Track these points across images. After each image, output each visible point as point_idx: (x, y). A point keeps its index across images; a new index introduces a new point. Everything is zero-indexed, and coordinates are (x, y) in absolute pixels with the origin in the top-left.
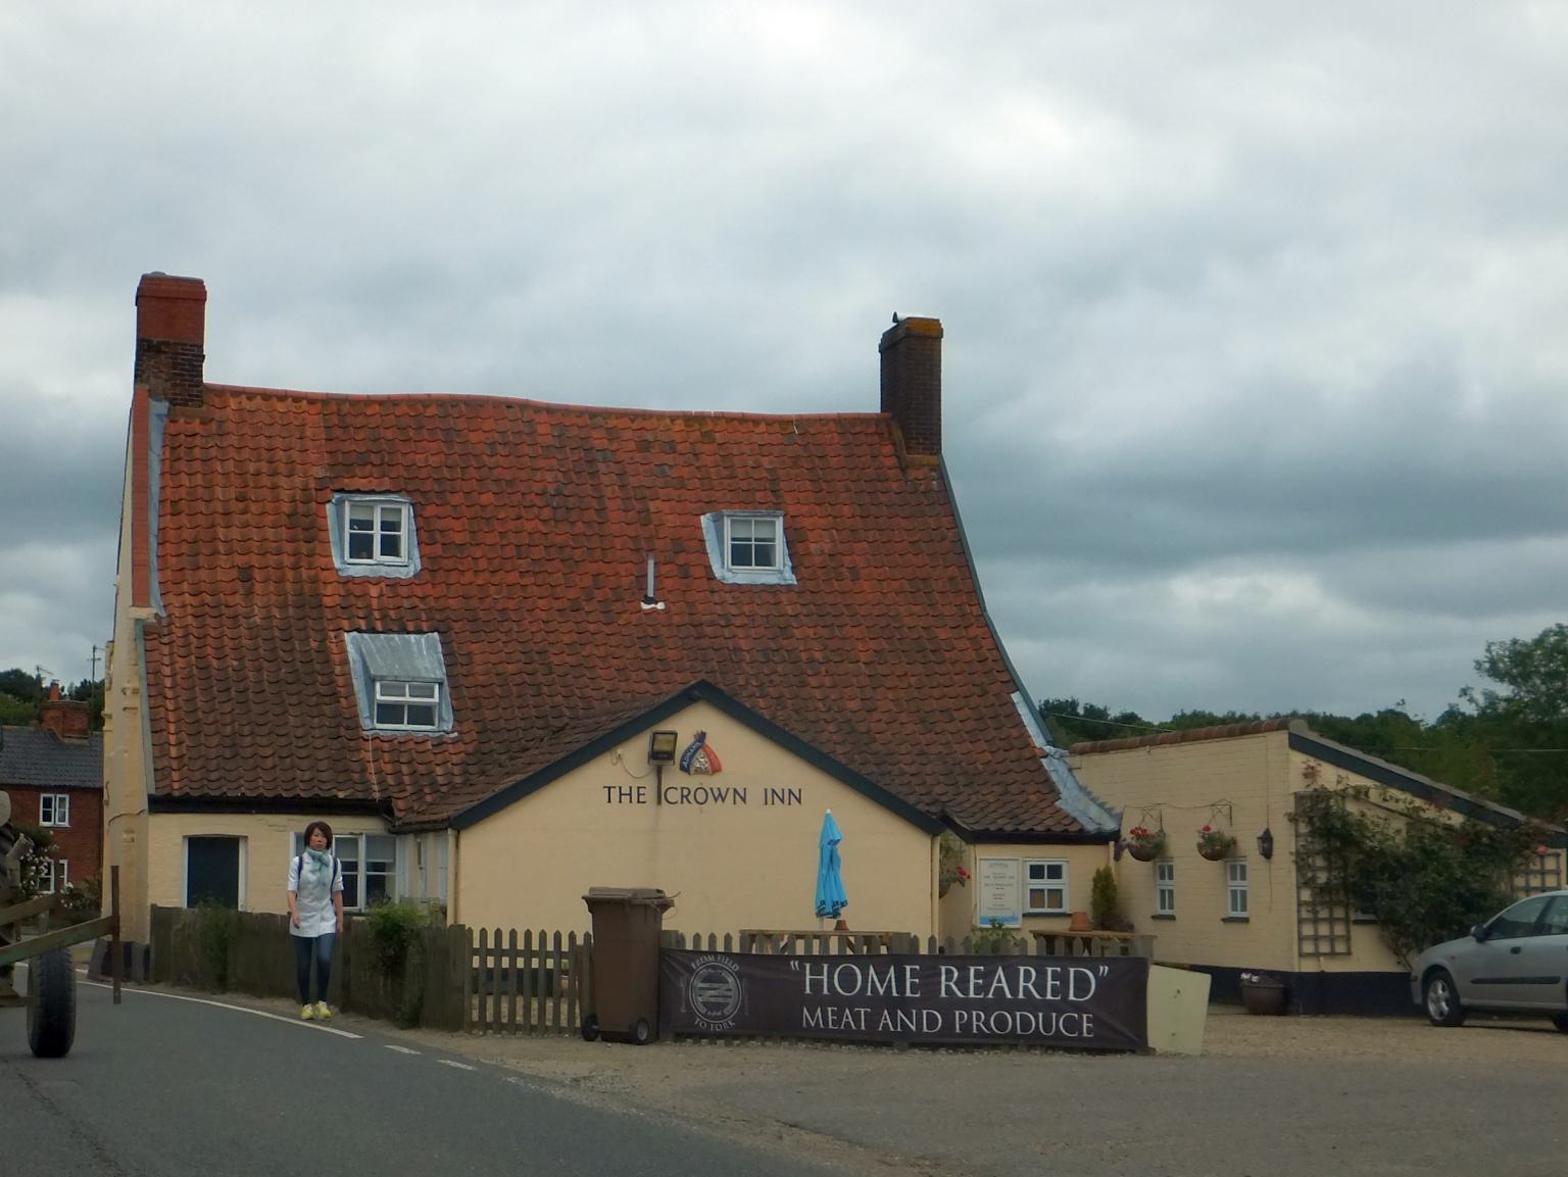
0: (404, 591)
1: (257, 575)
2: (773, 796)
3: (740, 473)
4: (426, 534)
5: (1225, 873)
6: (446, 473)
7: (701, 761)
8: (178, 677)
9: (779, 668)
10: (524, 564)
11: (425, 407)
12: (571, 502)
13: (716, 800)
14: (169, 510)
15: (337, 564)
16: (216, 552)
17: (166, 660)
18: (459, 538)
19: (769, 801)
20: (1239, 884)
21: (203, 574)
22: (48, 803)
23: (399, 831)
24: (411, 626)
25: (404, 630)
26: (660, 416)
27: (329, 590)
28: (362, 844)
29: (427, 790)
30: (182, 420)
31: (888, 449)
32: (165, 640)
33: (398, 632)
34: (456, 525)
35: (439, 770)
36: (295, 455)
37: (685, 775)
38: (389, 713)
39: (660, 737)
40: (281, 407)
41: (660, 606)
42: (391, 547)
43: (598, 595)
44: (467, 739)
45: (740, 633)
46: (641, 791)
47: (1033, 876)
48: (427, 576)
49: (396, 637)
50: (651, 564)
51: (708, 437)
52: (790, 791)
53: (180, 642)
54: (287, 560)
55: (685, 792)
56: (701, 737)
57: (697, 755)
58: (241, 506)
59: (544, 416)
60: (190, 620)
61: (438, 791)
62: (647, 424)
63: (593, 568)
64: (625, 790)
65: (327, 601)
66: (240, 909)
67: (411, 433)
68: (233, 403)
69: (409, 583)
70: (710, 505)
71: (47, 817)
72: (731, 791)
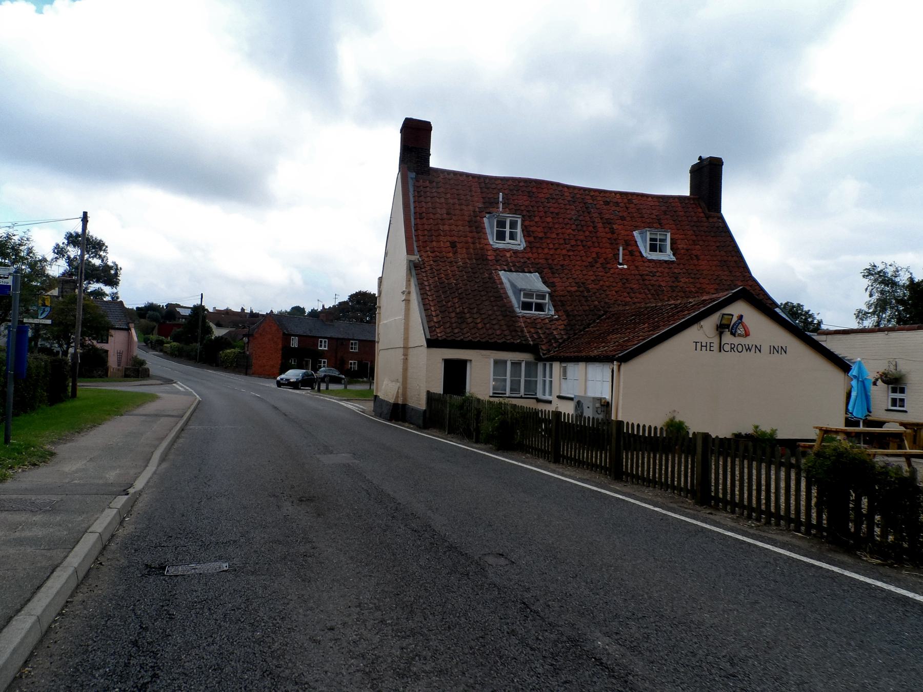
0: (520, 255)
1: (458, 245)
2: (774, 349)
3: (646, 216)
5: (888, 390)
6: (531, 208)
8: (432, 286)
9: (679, 294)
10: (568, 247)
11: (519, 182)
12: (583, 223)
13: (747, 350)
14: (418, 217)
15: (491, 243)
16: (439, 235)
17: (425, 279)
19: (772, 352)
20: (898, 396)
21: (434, 244)
22: (321, 342)
23: (539, 359)
24: (526, 270)
25: (523, 271)
26: (611, 192)
27: (489, 253)
28: (523, 365)
29: (553, 341)
30: (421, 181)
31: (700, 210)
32: (423, 270)
33: (521, 272)
34: (539, 229)
35: (555, 333)
36: (469, 198)
37: (733, 337)
38: (526, 306)
39: (726, 316)
42: (512, 237)
44: (563, 319)
45: (660, 279)
46: (712, 345)
48: (529, 249)
49: (521, 274)
50: (621, 249)
51: (630, 202)
52: (782, 347)
53: (430, 271)
54: (470, 240)
55: (733, 346)
57: (739, 327)
58: (449, 217)
59: (566, 189)
60: (432, 262)
61: (558, 342)
62: (607, 195)
63: (597, 249)
64: (704, 344)
65: (489, 258)
67: (515, 192)
69: (522, 252)
70: (636, 228)
71: (352, 348)
72: (754, 346)
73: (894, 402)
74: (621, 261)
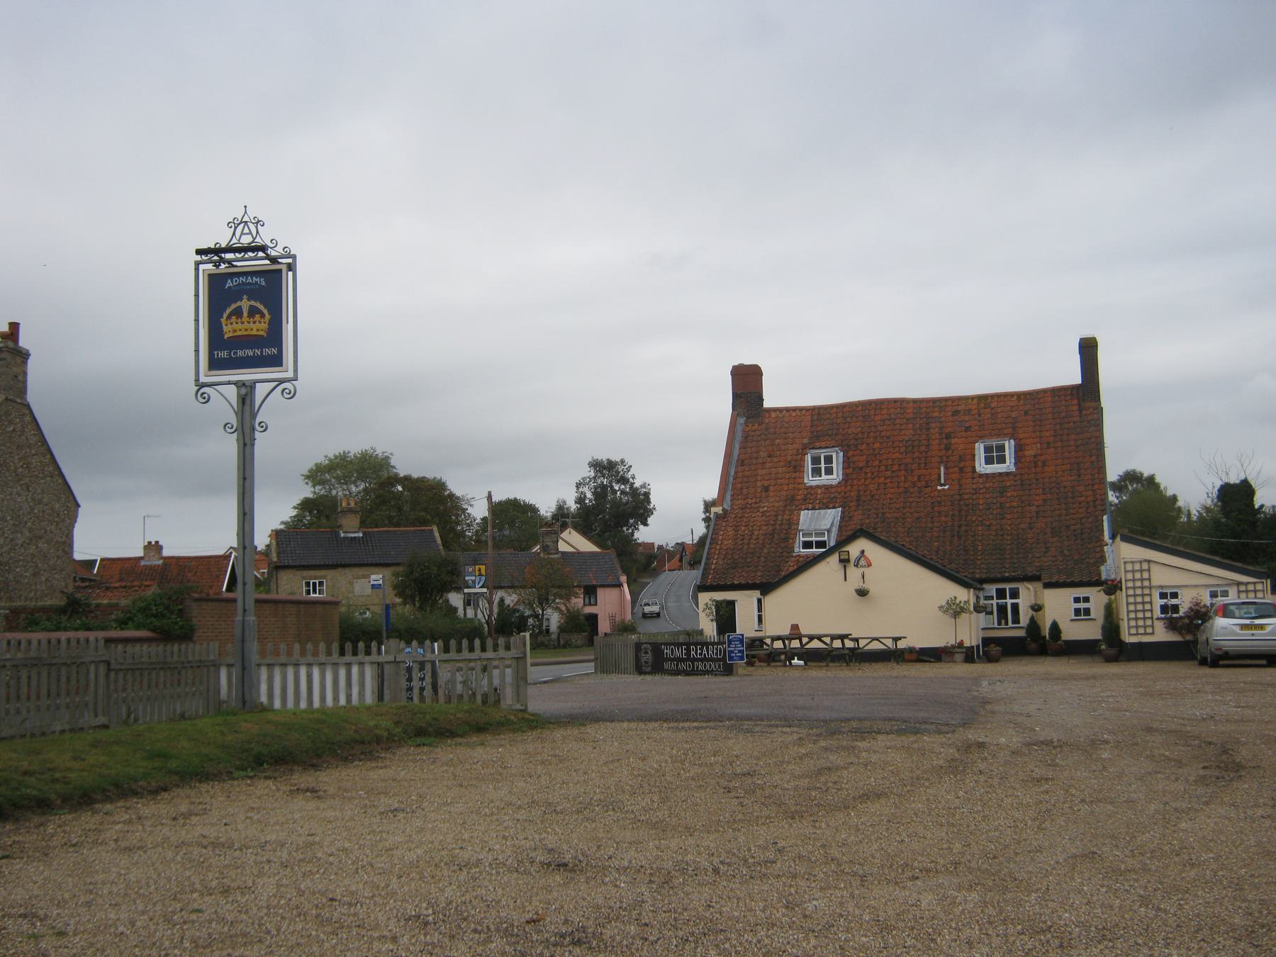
4: (847, 463)
7: (863, 562)
10: (889, 473)
11: (857, 407)
18: (861, 465)
40: (794, 414)
41: (947, 487)
42: (829, 471)
43: (919, 484)
47: (1075, 602)
50: (942, 468)
56: (863, 552)
58: (769, 459)
66: (1099, 637)
68: (773, 415)
73: (1077, 612)
74: (942, 482)
